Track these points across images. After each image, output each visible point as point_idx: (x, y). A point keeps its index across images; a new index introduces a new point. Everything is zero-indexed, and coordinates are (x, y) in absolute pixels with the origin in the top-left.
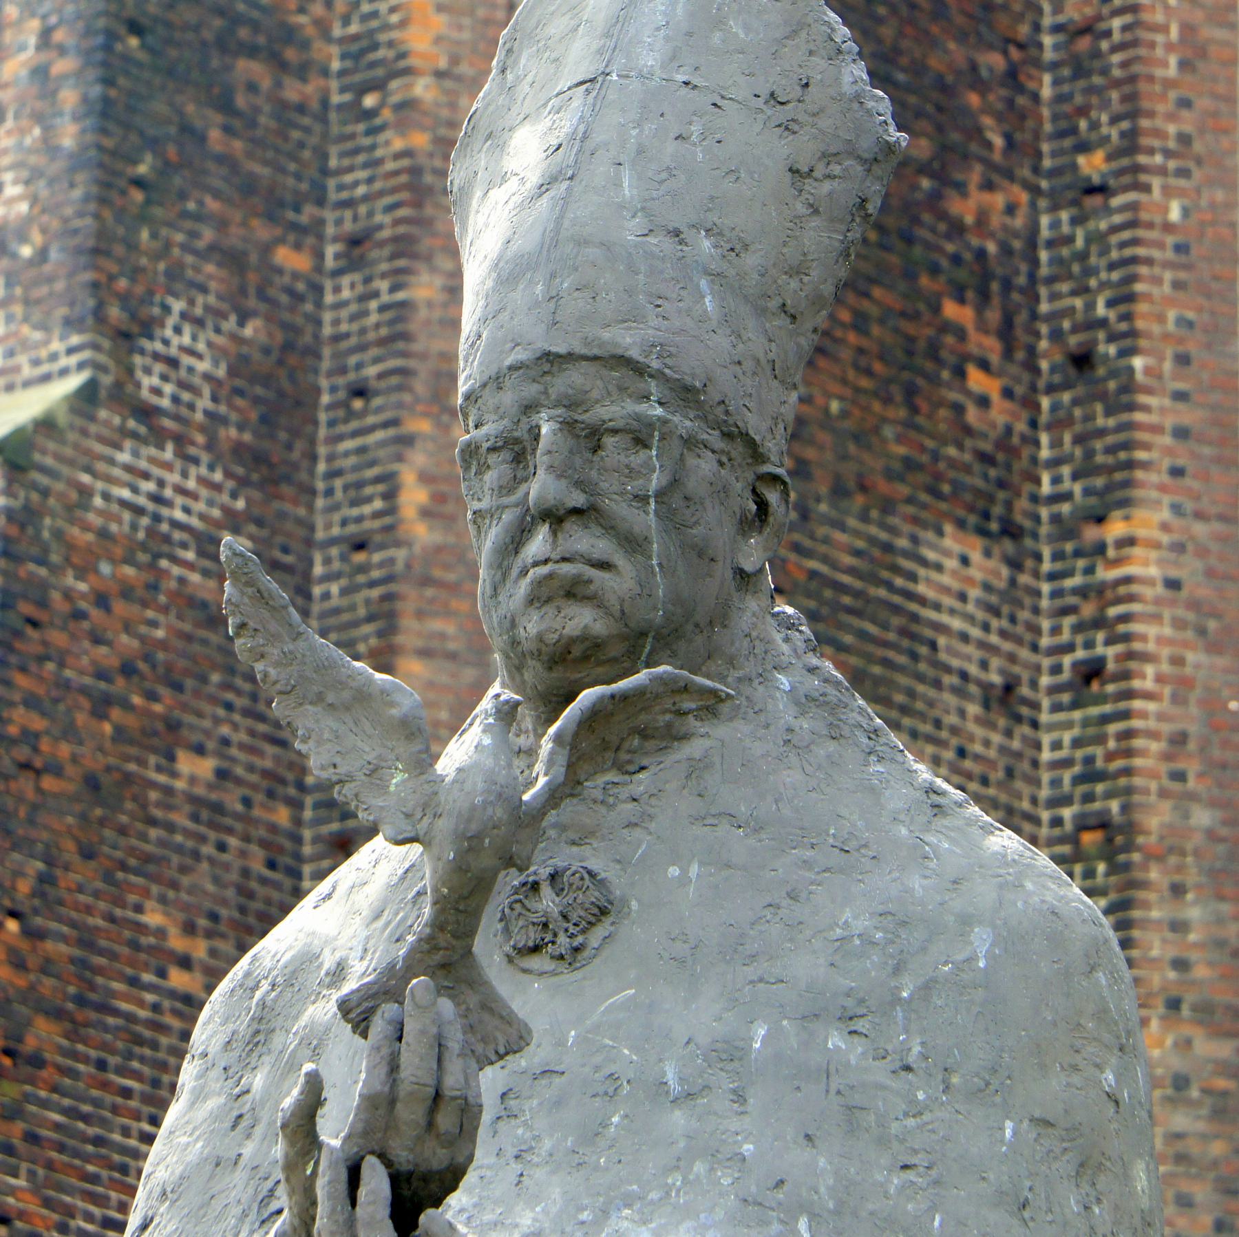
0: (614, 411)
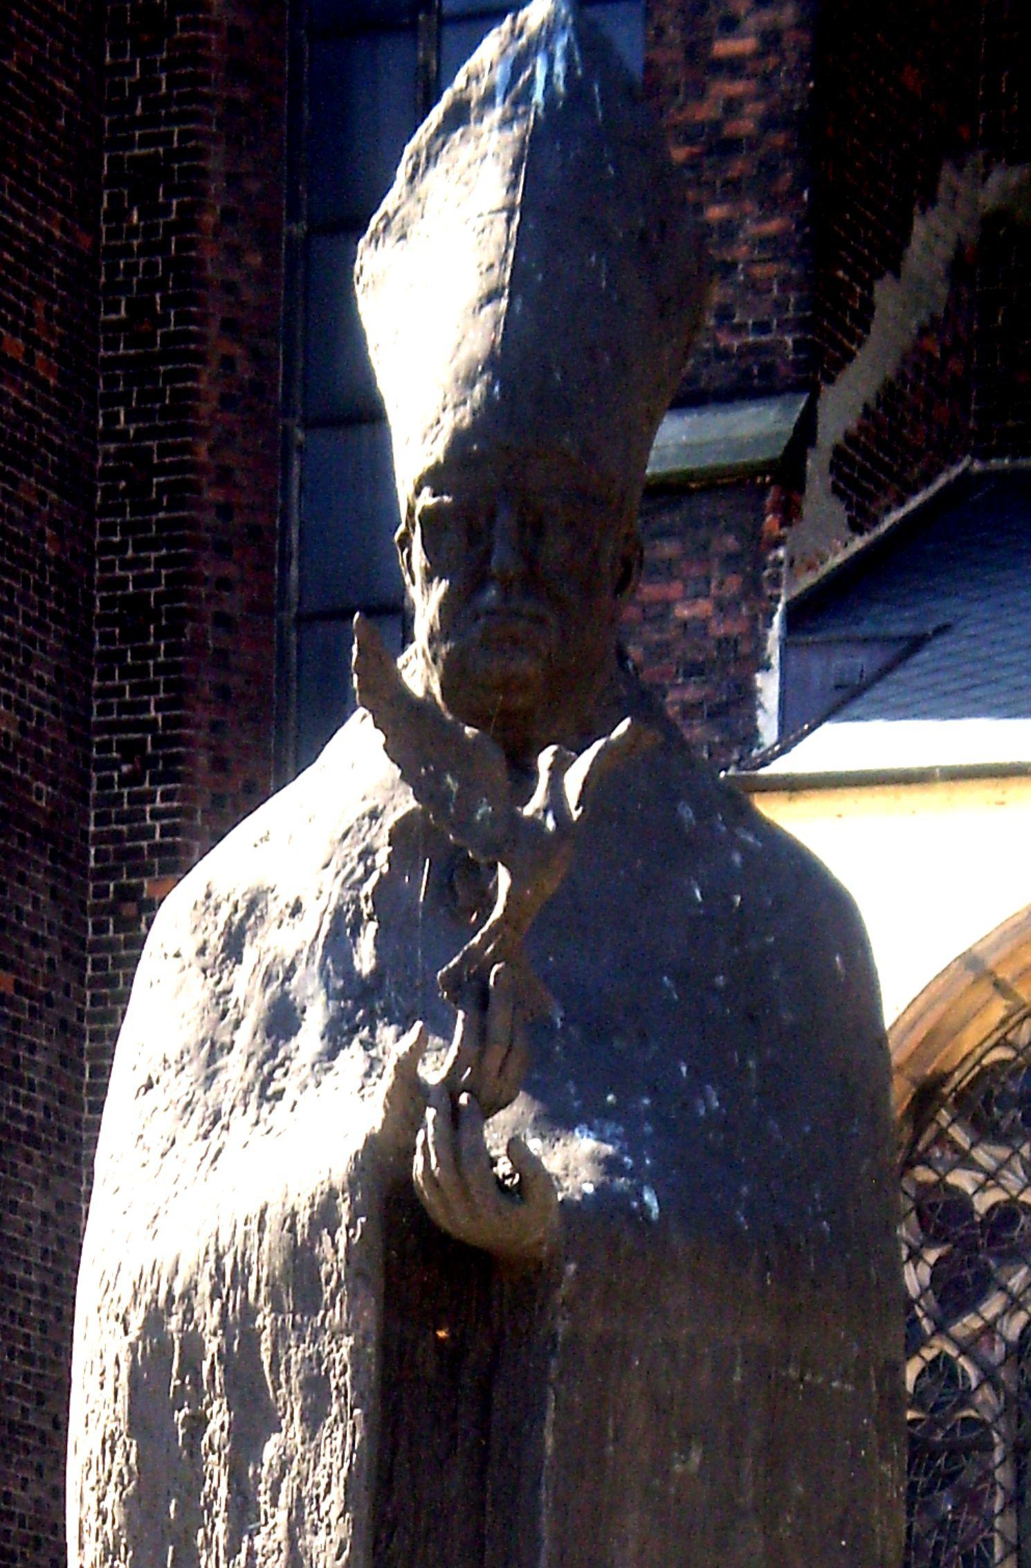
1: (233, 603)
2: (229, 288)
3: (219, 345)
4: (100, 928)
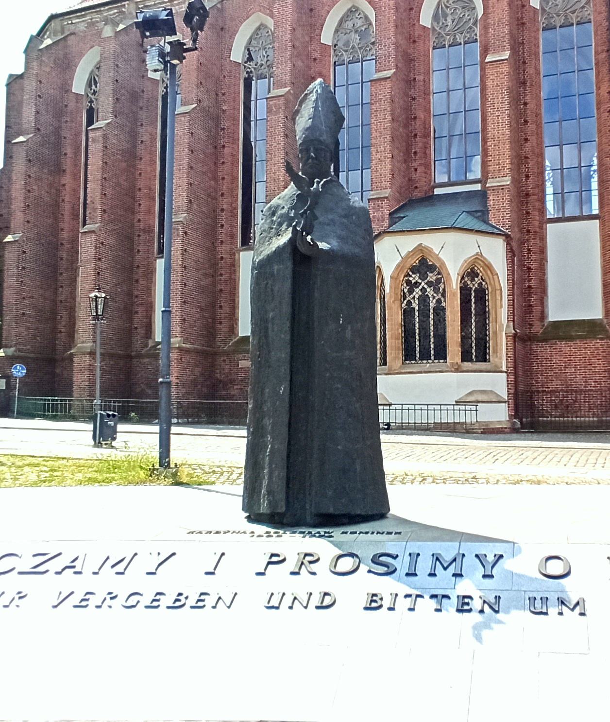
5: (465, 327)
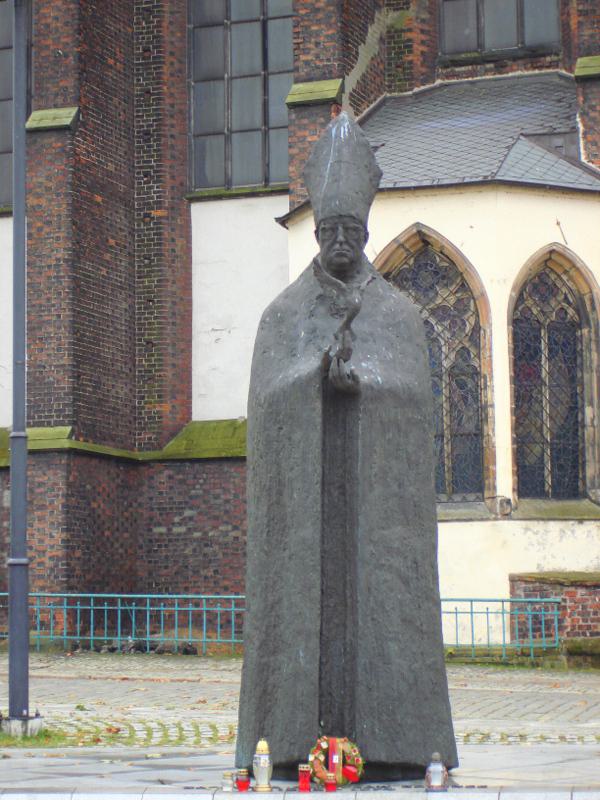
0: (352, 225)
1: (174, 131)
2: (172, 43)
3: (168, 59)
4: (139, 225)
5: (526, 415)
